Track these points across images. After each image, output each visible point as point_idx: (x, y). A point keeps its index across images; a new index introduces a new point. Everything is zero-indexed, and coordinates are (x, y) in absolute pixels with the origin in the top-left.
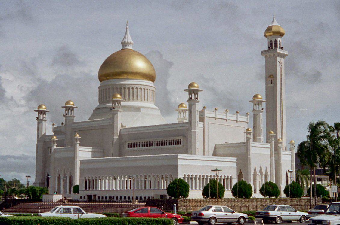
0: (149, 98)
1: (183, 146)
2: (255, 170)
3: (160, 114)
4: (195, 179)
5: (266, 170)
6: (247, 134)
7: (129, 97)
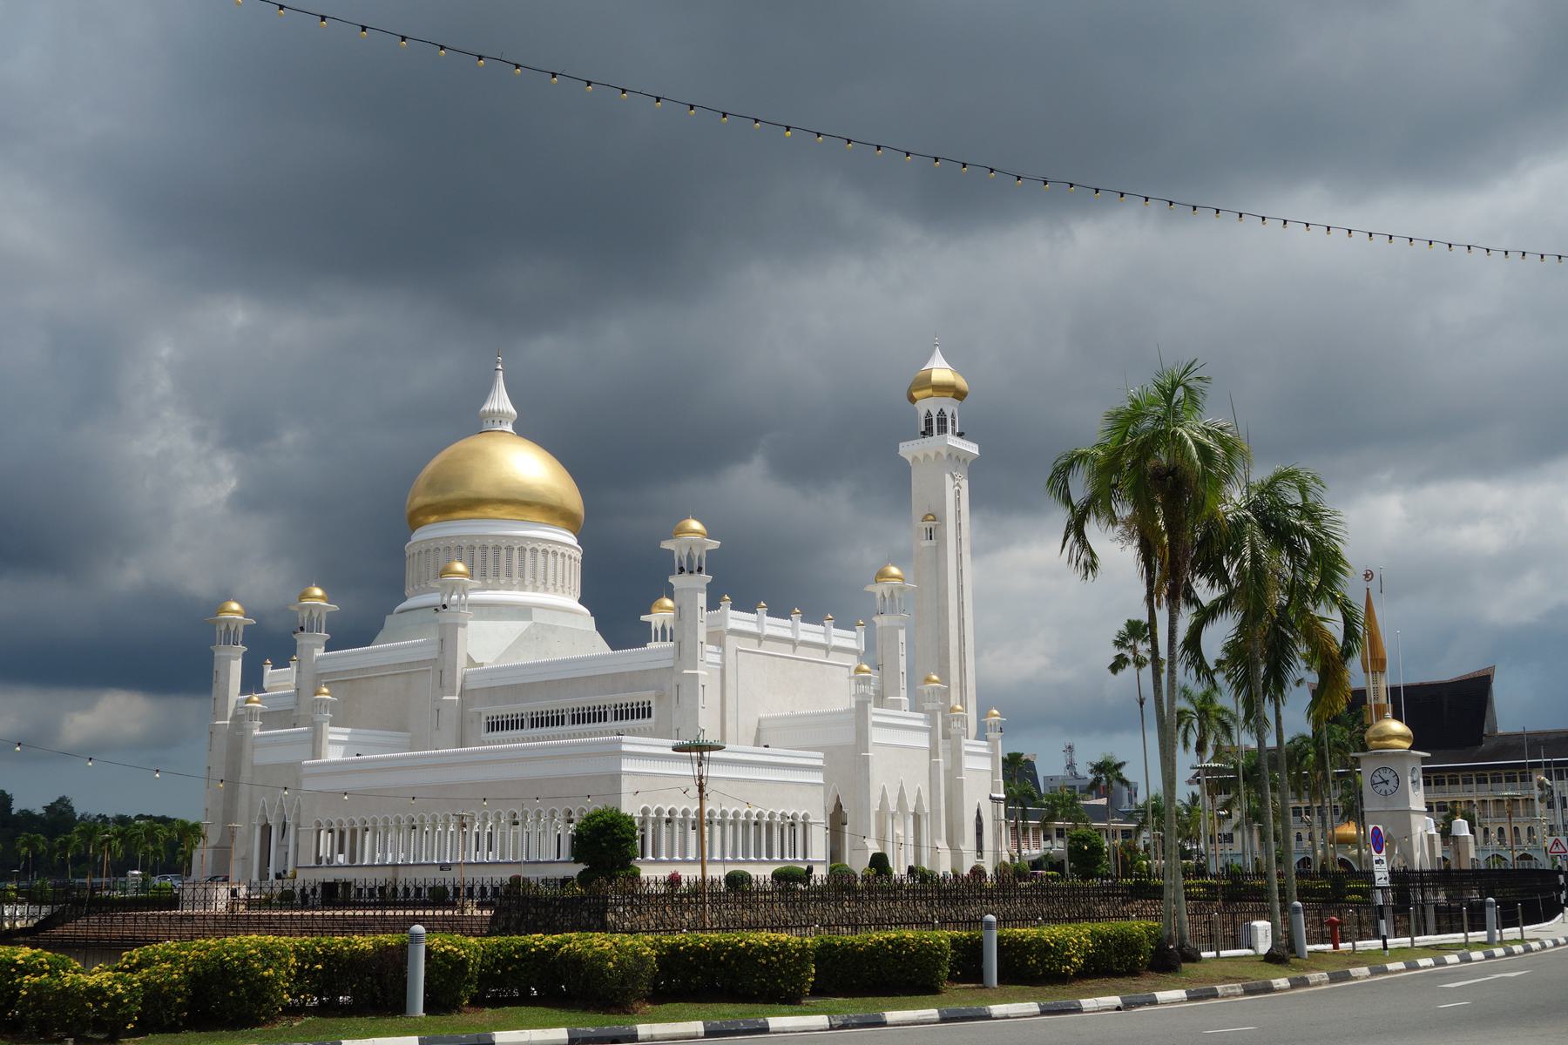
0: (559, 579)
1: (657, 723)
2: (884, 797)
3: (1377, 522)
4: (746, 825)
5: (919, 798)
6: (858, 683)
7: (522, 576)
